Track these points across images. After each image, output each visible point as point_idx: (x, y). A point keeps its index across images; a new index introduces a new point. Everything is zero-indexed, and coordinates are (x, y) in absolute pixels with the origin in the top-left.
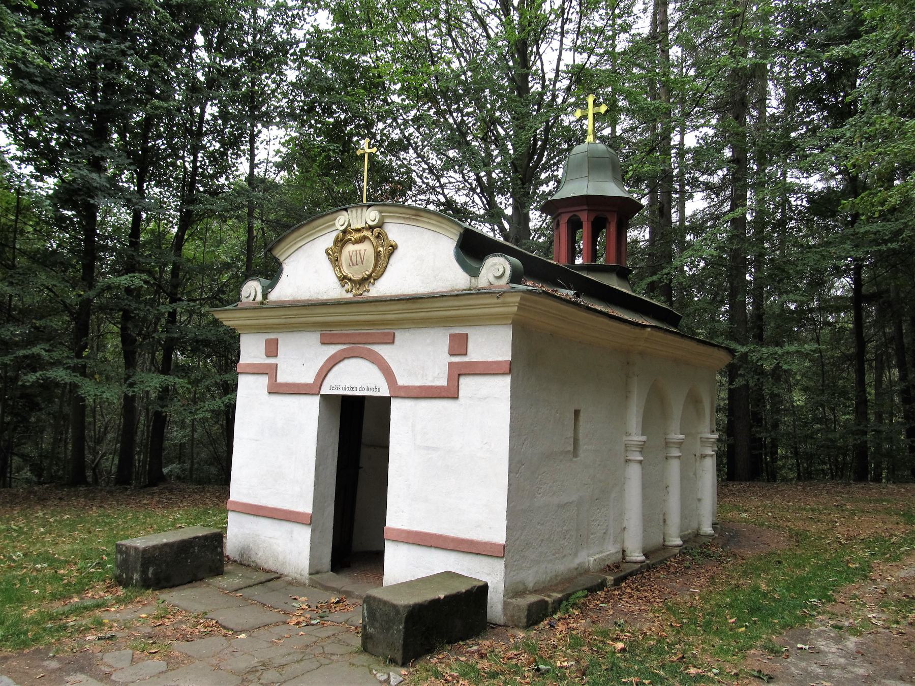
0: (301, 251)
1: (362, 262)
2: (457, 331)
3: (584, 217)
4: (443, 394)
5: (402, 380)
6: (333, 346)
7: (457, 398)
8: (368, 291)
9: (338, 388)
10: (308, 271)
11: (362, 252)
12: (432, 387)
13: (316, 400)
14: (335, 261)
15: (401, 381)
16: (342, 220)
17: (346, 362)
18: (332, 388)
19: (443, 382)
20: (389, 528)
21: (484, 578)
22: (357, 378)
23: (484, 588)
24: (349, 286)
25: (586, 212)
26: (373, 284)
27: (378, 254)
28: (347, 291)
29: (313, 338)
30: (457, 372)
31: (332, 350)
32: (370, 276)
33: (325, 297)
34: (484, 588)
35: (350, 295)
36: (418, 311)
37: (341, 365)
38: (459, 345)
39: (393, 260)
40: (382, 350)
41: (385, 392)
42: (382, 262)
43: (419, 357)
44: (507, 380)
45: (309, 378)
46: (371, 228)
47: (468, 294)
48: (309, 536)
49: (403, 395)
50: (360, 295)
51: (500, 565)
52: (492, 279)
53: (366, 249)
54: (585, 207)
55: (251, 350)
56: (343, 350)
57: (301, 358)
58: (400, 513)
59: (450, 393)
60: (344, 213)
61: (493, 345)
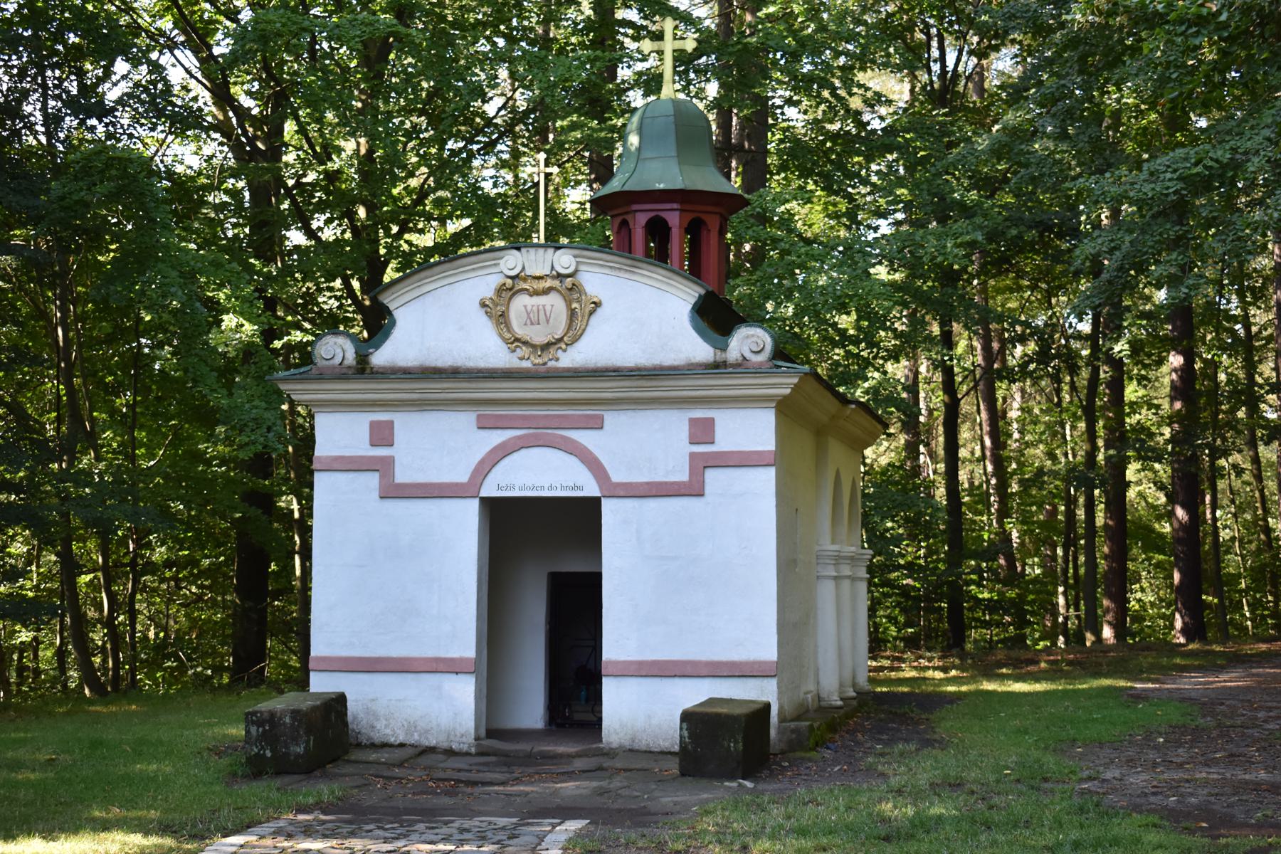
0: (429, 298)
1: (548, 321)
2: (700, 414)
3: (674, 219)
4: (683, 491)
5: (618, 475)
6: (499, 432)
7: (701, 494)
8: (557, 359)
9: (542, 488)
10: (440, 321)
11: (548, 308)
12: (666, 483)
13: (474, 505)
14: (501, 320)
15: (616, 477)
16: (512, 262)
17: (523, 452)
18: (499, 488)
19: (682, 476)
20: (610, 662)
21: (764, 699)
22: (541, 474)
23: (767, 706)
24: (525, 351)
25: (677, 213)
26: (565, 351)
27: (572, 314)
28: (521, 359)
29: (466, 420)
30: (701, 465)
31: (498, 437)
32: (561, 340)
33: (482, 364)
34: (767, 706)
35: (526, 364)
36: (643, 384)
37: (515, 456)
38: (701, 432)
39: (594, 319)
40: (584, 438)
41: (598, 494)
42: (578, 323)
43: (642, 443)
44: (771, 472)
45: (461, 475)
46: (560, 276)
47: (717, 367)
48: (473, 688)
49: (622, 493)
50: (545, 364)
51: (773, 683)
52: (748, 355)
53: (555, 303)
54: (675, 206)
55: (337, 434)
56: (519, 437)
57: (440, 445)
58: (617, 642)
59: (693, 489)
60: (515, 252)
61: (753, 429)
